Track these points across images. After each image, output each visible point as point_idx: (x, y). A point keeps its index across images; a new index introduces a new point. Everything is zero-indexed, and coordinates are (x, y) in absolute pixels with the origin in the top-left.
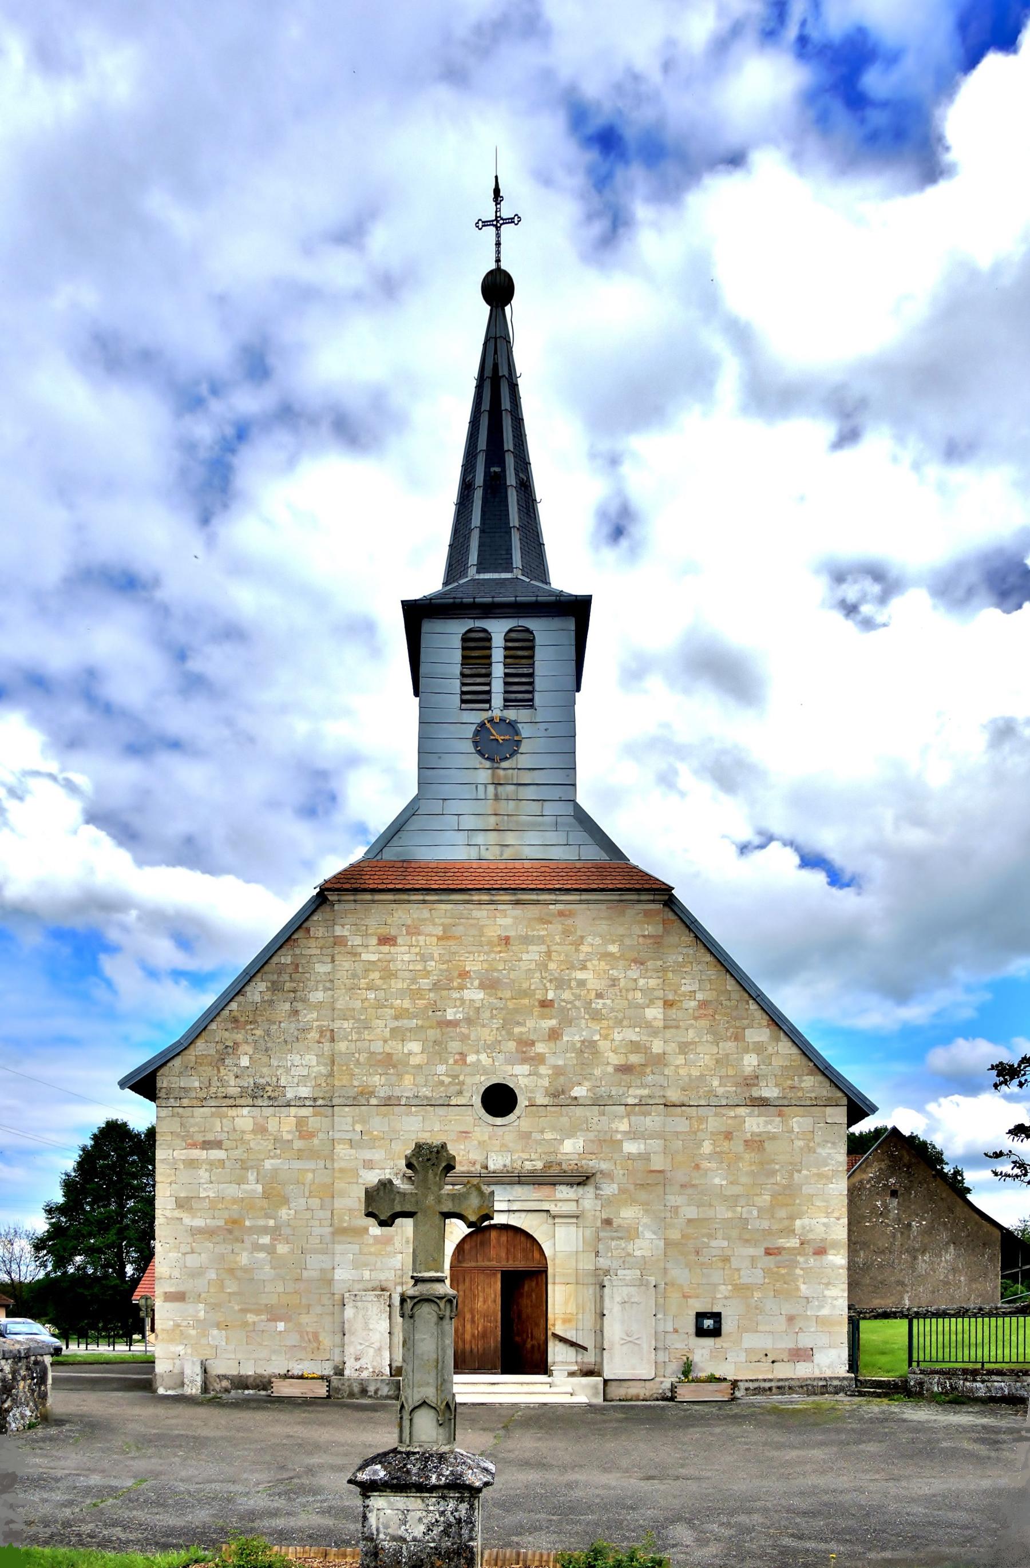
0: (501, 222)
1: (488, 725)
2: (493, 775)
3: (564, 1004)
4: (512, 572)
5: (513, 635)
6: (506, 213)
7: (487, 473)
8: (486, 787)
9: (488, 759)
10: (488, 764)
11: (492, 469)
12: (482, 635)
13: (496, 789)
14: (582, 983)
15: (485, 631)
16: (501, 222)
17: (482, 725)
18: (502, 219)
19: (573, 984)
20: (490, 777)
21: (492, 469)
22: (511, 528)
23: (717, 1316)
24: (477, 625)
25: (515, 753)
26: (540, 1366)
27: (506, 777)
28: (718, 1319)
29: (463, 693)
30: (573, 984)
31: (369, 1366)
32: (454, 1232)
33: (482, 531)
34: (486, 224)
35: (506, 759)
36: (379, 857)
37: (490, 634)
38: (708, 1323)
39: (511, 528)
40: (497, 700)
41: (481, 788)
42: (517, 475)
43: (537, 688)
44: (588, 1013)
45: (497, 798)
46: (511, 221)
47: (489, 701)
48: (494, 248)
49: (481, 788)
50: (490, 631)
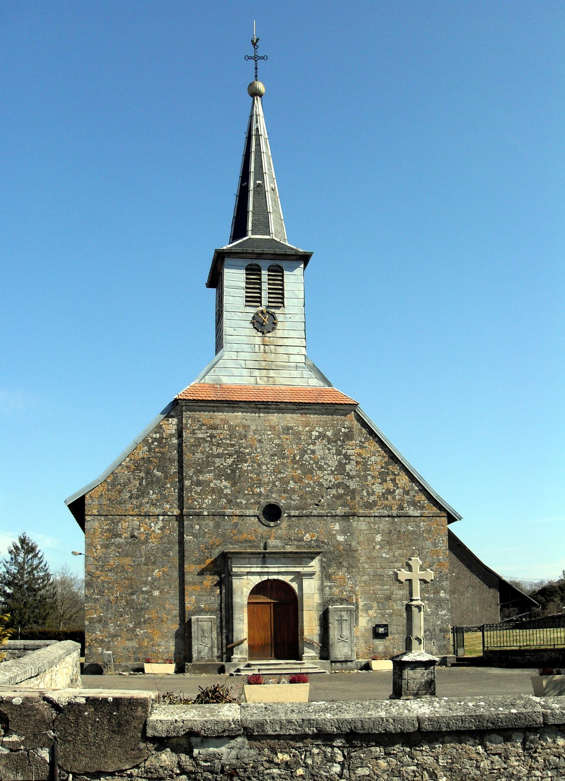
0: (258, 58)
1: (260, 315)
2: (263, 340)
3: (304, 462)
4: (270, 235)
5: (271, 268)
6: (260, 54)
7: (255, 183)
8: (259, 346)
9: (260, 332)
10: (260, 334)
11: (258, 182)
12: (256, 267)
13: (265, 347)
14: (313, 452)
15: (258, 265)
16: (258, 58)
17: (257, 314)
18: (258, 57)
19: (309, 452)
20: (261, 341)
21: (258, 182)
22: (259, 135)
23: (385, 626)
24: (253, 262)
25: (274, 329)
26: (297, 655)
27: (270, 341)
28: (386, 628)
29: (247, 297)
30: (309, 452)
31: (206, 656)
32: (250, 584)
33: (253, 213)
34: (250, 58)
35: (269, 332)
36: (202, 381)
37: (260, 267)
38: (381, 630)
39: (259, 135)
40: (265, 302)
41: (257, 346)
42: (270, 185)
43: (286, 296)
44: (317, 467)
45: (265, 352)
46: (263, 58)
47: (260, 302)
48: (254, 70)
49: (257, 346)
50: (260, 265)
